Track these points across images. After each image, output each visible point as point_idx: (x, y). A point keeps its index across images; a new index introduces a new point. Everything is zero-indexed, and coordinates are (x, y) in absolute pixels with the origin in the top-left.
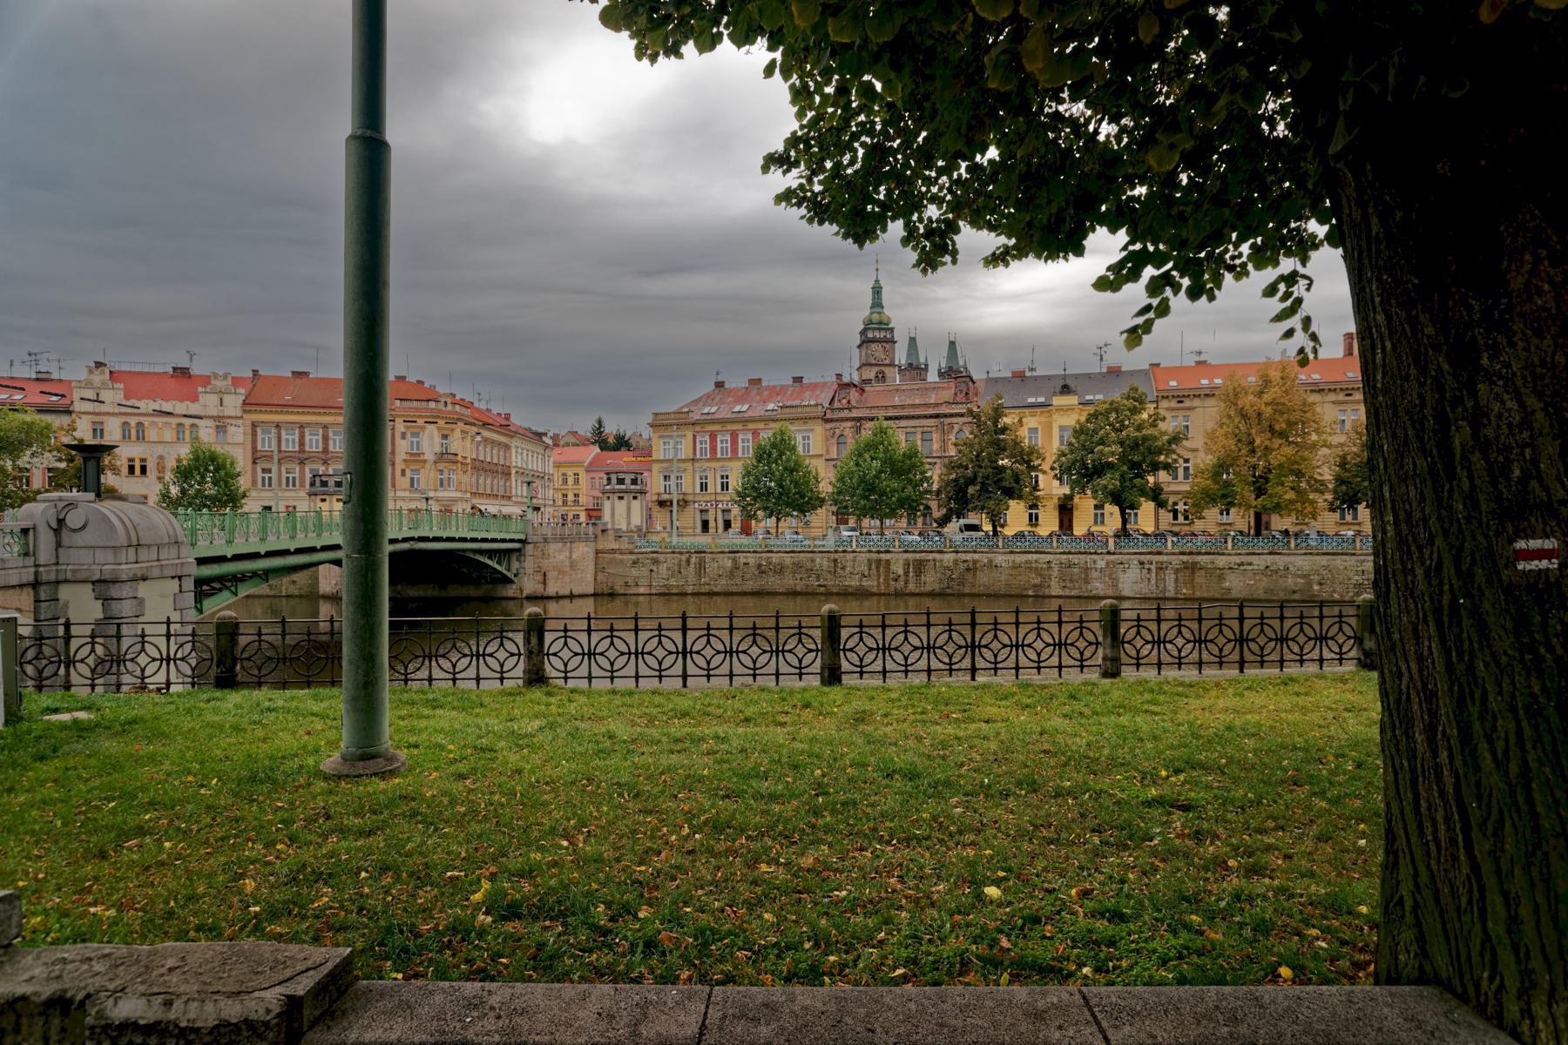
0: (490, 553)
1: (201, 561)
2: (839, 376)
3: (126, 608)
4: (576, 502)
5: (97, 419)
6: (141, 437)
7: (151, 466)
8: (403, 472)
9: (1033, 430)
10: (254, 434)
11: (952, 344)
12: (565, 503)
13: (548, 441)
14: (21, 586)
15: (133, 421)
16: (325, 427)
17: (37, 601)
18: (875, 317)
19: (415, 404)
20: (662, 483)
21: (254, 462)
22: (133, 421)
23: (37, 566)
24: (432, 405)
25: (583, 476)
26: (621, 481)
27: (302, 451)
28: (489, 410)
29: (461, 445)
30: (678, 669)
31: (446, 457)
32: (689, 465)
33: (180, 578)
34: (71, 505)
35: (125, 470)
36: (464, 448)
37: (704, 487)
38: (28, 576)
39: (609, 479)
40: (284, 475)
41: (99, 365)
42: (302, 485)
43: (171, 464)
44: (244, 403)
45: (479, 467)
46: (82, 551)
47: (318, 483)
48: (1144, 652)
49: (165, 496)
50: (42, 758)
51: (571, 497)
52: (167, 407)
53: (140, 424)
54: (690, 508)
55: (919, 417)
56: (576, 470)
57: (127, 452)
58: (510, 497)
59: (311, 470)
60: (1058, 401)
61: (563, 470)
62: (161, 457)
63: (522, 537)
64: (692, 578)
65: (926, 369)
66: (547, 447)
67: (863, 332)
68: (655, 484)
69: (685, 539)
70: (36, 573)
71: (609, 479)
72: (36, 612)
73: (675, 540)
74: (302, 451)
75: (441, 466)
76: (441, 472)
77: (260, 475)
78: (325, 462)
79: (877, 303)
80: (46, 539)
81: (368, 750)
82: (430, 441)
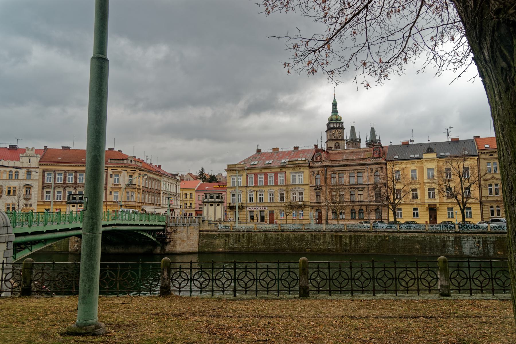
0: (149, 232)
1: (17, 235)
2: (316, 146)
4: (191, 207)
8: (111, 192)
9: (413, 171)
10: (44, 176)
11: (373, 129)
12: (186, 208)
13: (179, 178)
16: (76, 172)
18: (334, 117)
19: (117, 161)
21: (43, 189)
24: (125, 162)
25: (194, 195)
26: (212, 197)
27: (65, 183)
28: (151, 164)
29: (137, 180)
31: (130, 186)
32: (244, 189)
33: (7, 242)
36: (139, 182)
37: (251, 199)
39: (206, 196)
44: (40, 161)
45: (146, 191)
47: (71, 198)
51: (188, 205)
54: (244, 210)
55: (355, 165)
59: (69, 192)
60: (426, 156)
61: (185, 192)
63: (164, 223)
64: (245, 245)
65: (360, 142)
66: (178, 181)
67: (328, 125)
68: (229, 199)
69: (242, 225)
71: (206, 196)
73: (237, 225)
74: (65, 183)
75: (128, 190)
77: (45, 194)
78: (75, 189)
79: (335, 111)
82: (124, 179)
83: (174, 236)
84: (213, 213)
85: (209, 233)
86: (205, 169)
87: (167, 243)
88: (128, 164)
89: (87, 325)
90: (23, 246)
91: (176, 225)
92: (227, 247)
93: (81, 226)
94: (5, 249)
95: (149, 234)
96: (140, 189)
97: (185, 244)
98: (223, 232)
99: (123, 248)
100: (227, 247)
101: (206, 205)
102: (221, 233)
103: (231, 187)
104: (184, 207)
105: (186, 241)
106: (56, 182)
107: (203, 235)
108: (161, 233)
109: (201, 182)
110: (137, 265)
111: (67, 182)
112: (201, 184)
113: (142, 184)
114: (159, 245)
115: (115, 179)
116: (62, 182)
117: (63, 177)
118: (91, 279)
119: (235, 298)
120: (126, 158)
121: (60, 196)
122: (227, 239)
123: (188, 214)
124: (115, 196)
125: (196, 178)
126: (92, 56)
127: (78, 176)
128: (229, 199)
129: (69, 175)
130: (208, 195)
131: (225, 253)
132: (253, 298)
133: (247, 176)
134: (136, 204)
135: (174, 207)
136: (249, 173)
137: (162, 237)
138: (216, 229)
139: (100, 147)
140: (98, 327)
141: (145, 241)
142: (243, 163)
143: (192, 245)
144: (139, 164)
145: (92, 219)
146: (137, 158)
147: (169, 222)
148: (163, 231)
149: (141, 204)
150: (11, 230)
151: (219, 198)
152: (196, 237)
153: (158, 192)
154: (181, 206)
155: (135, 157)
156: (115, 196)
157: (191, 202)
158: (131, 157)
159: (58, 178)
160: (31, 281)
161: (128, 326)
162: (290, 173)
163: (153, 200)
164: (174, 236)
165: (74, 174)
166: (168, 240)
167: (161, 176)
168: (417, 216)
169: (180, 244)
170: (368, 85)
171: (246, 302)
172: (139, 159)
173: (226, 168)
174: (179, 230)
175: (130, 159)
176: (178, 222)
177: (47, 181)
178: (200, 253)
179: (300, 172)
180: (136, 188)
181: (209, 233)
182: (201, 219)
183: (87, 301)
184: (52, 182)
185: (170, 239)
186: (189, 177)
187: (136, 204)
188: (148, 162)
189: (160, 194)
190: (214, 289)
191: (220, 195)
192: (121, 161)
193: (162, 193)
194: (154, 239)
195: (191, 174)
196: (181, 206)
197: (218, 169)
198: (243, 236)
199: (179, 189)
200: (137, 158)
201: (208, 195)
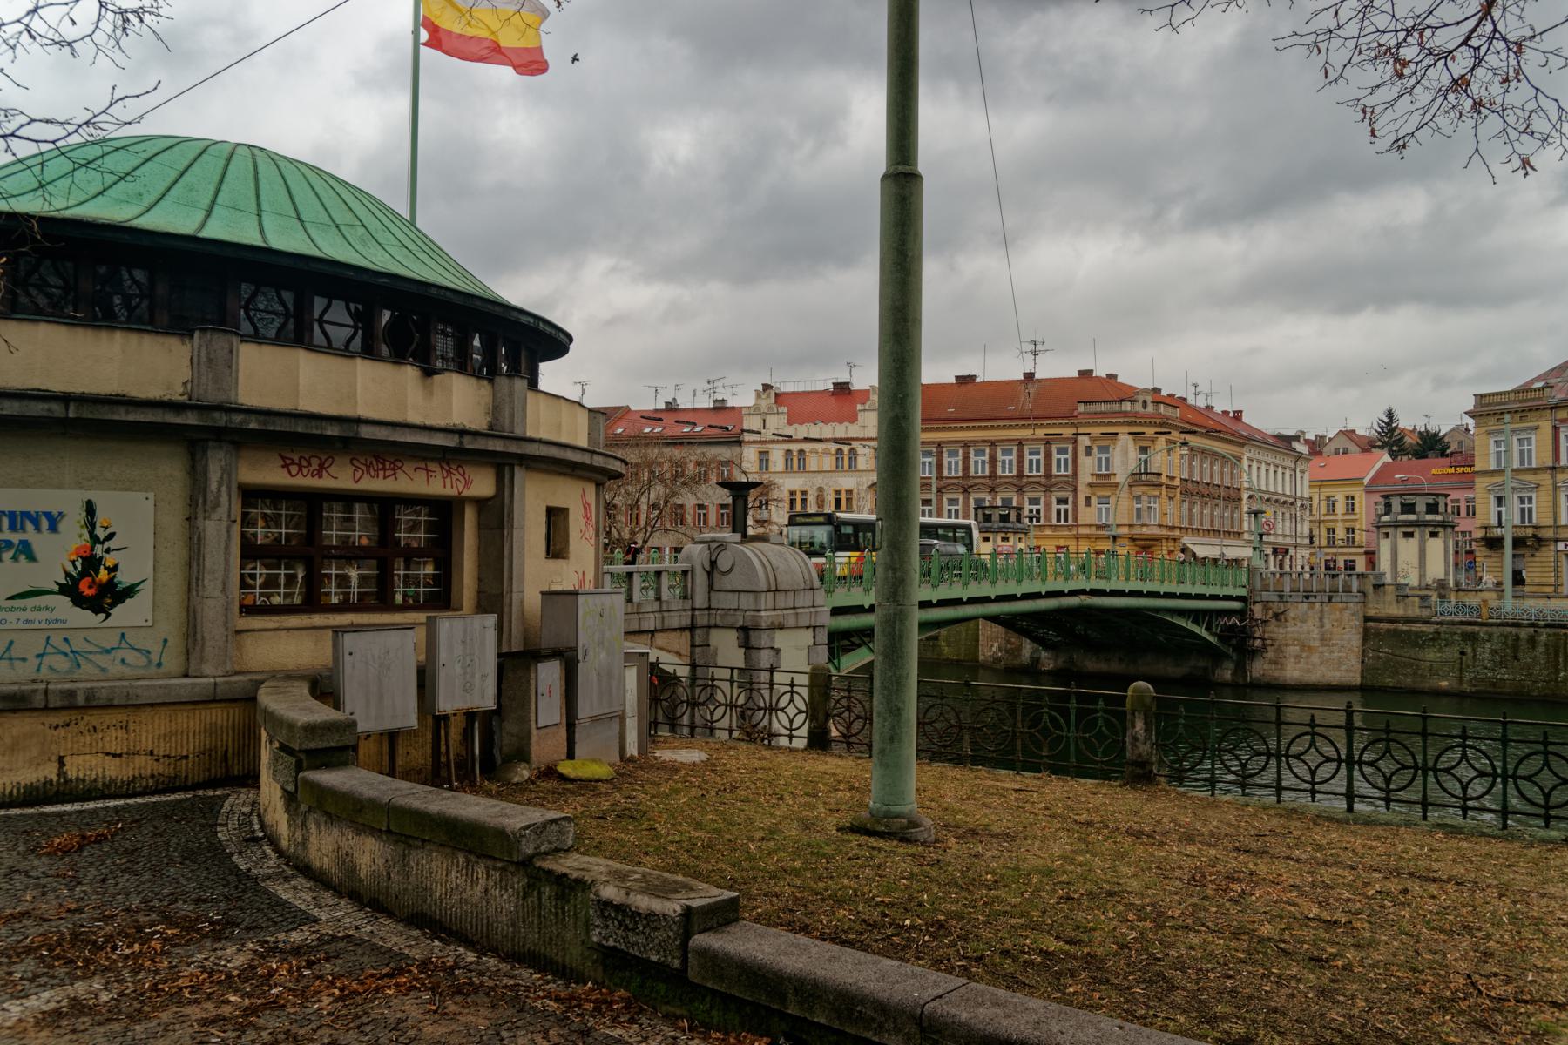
0: (1196, 615)
1: (836, 611)
4: (1350, 542)
5: (764, 447)
6: (802, 468)
8: (1088, 499)
12: (1331, 542)
13: (1301, 448)
17: (693, 646)
19: (1103, 407)
20: (1494, 508)
23: (693, 609)
24: (1127, 406)
25: (1361, 501)
26: (1408, 508)
27: (966, 476)
28: (1210, 408)
30: (1339, 784)
31: (1143, 478)
32: (1545, 479)
34: (722, 546)
36: (1171, 464)
38: (685, 620)
39: (1388, 507)
41: (767, 387)
45: (1193, 491)
46: (730, 595)
48: (1537, 762)
51: (1341, 533)
56: (1350, 491)
58: (1239, 534)
59: (976, 501)
61: (1327, 491)
63: (1243, 592)
66: (1299, 457)
69: (1530, 603)
70: (693, 616)
71: (1388, 507)
74: (966, 476)
75: (1138, 490)
76: (1138, 498)
78: (992, 490)
80: (701, 579)
81: (893, 808)
82: (1124, 457)
83: (1274, 630)
84: (1417, 561)
85: (1400, 626)
86: (1397, 414)
87: (1255, 653)
88: (1136, 415)
89: (889, 816)
90: (856, 640)
91: (1281, 597)
92: (1467, 676)
95: (1196, 622)
96: (1175, 488)
97: (1315, 659)
98: (1453, 623)
99: (1121, 660)
100: (1467, 676)
101: (1387, 535)
102: (1444, 628)
103: (1492, 473)
104: (1324, 542)
105: (1318, 648)
106: (946, 473)
107: (1371, 630)
108: (1235, 620)
109: (1387, 458)
110: (1064, 697)
111: (972, 473)
112: (1386, 465)
113: (1180, 473)
114: (1228, 657)
115: (1100, 460)
117: (1014, 457)
118: (896, 712)
119: (1350, 816)
120: (1128, 395)
122: (1469, 650)
123: (1341, 564)
124: (1100, 510)
125: (1368, 446)
127: (1000, 457)
128: (1488, 511)
129: (977, 453)
130: (1396, 504)
131: (1460, 696)
132: (1408, 824)
133: (1556, 429)
134: (1164, 532)
135: (1288, 540)
136: (1563, 421)
137: (1238, 632)
138: (1425, 613)
139: (906, 396)
140: (914, 824)
141: (1187, 645)
142: (1539, 385)
143: (1340, 663)
144: (1170, 412)
145: (894, 570)
146: (1164, 393)
147: (1258, 585)
148: (1241, 614)
149: (1177, 532)
150: (820, 597)
151: (1437, 512)
152: (1352, 638)
153: (1233, 494)
154: (1311, 537)
155: (1156, 391)
156: (1100, 510)
157: (1348, 524)
158: (1146, 391)
160: (828, 716)
161: (995, 836)
162: (1489, 433)
163: (1217, 521)
164: (1274, 630)
166: (1258, 643)
167: (1242, 445)
169: (1298, 657)
170: (1526, 163)
171: (1379, 831)
172: (1171, 396)
173: (1471, 407)
174: (1291, 614)
175: (1141, 398)
176: (1287, 589)
177: (1031, 470)
178: (1366, 690)
179: (1522, 430)
180: (1160, 485)
181: (1400, 626)
182: (1371, 580)
183: (892, 767)
184: (934, 476)
185: (1263, 639)
186: (1344, 443)
187: (1164, 532)
188: (1201, 403)
189: (1240, 500)
190: (1284, 783)
191: (1441, 501)
192: (1116, 407)
193: (1245, 496)
194: (1211, 639)
195: (1349, 434)
196: (1311, 537)
197: (1446, 412)
198: (1532, 641)
199: (1306, 483)
200: (1164, 393)
201: (1396, 504)
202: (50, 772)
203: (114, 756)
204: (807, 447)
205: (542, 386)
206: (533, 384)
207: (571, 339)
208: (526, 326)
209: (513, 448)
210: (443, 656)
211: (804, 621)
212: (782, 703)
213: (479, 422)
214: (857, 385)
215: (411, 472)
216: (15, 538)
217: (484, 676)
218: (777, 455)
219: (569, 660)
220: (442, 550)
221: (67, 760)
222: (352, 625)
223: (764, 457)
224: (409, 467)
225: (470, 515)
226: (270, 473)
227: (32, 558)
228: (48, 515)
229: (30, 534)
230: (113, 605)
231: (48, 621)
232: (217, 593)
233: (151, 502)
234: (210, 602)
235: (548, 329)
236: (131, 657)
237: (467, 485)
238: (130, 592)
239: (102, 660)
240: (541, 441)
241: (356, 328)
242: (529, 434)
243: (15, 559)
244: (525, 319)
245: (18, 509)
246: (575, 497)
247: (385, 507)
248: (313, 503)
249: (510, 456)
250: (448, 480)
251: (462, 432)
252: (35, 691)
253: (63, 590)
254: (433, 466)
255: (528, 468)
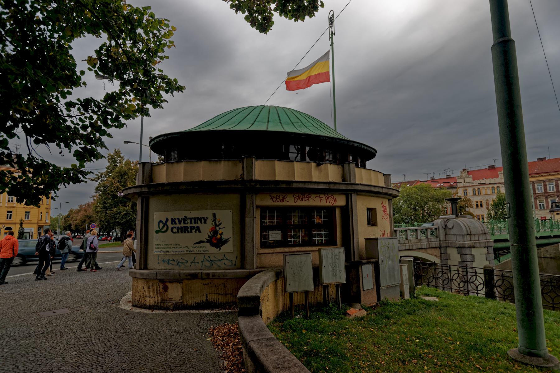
1: (496, 241)
3: (468, 258)
5: (465, 189)
6: (479, 193)
7: (484, 204)
14: (436, 248)
15: (476, 188)
16: (544, 182)
22: (476, 188)
33: (487, 247)
34: (448, 220)
35: (475, 206)
38: (438, 245)
40: (538, 204)
41: (464, 170)
42: (548, 207)
43: (491, 202)
46: (453, 236)
47: (554, 206)
49: (489, 215)
50: (409, 314)
52: (483, 181)
53: (479, 189)
57: (475, 200)
59: (551, 200)
62: (487, 200)
72: (441, 257)
80: (442, 232)
93: (508, 237)
94: (487, 252)
106: (537, 192)
111: (548, 191)
116: (543, 192)
121: (543, 205)
126: (492, 43)
159: (538, 189)
165: (554, 183)
168: (10, 218)
202: (204, 299)
203: (221, 295)
204: (481, 187)
205: (367, 167)
206: (363, 166)
207: (376, 151)
208: (357, 147)
209: (350, 187)
210: (324, 263)
211: (483, 245)
212: (454, 278)
213: (338, 180)
214: (497, 166)
215: (314, 198)
216: (195, 225)
217: (340, 271)
218: (470, 191)
219: (377, 266)
220: (330, 226)
221: (208, 295)
222: (298, 251)
223: (465, 193)
224: (313, 196)
225: (338, 212)
226: (267, 201)
227: (200, 232)
228: (204, 218)
229: (199, 224)
230: (222, 246)
231: (204, 251)
232: (250, 241)
233: (231, 213)
234: (248, 244)
235: (366, 148)
236: (227, 262)
237: (335, 201)
238: (226, 241)
239: (219, 263)
240: (374, 186)
241: (298, 154)
242: (357, 183)
243: (195, 232)
244: (356, 145)
245: (196, 216)
246: (381, 206)
247: (308, 211)
248: (286, 211)
249: (349, 191)
250: (328, 200)
251: (330, 183)
252: (199, 273)
253: (208, 241)
254: (322, 196)
255: (357, 195)
